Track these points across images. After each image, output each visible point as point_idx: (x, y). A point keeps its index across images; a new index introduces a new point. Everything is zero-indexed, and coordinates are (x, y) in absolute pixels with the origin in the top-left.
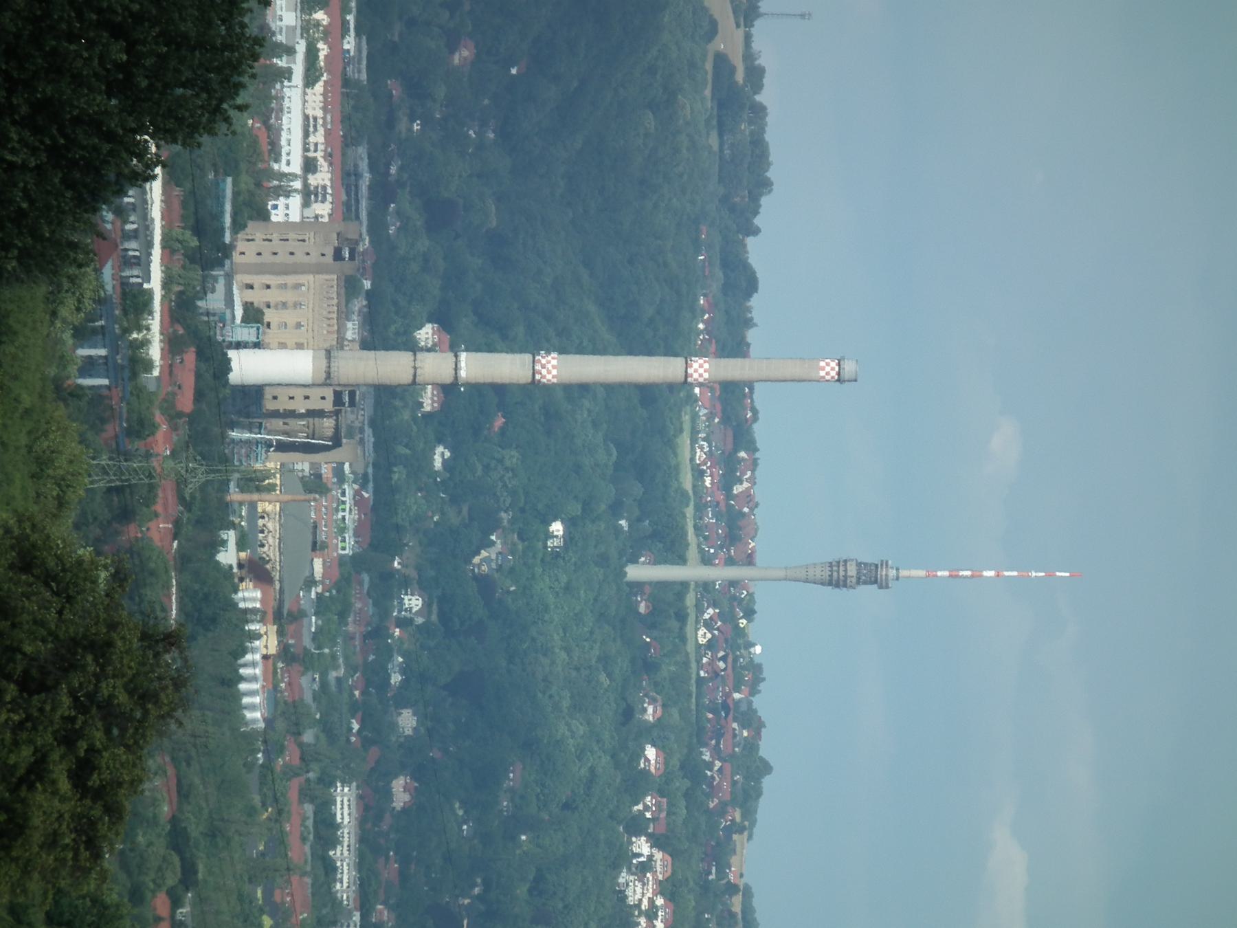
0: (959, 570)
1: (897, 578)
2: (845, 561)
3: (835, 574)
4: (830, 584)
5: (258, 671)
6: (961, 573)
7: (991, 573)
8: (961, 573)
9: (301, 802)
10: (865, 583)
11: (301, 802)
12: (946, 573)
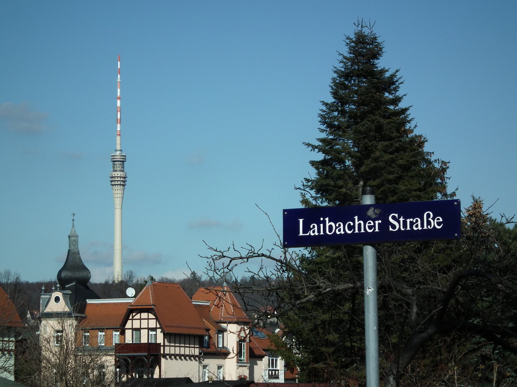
0: (117, 119)
1: (121, 151)
2: (124, 185)
3: (119, 183)
4: (430, 153)
5: (425, 228)
6: (119, 117)
7: (119, 102)
8: (119, 117)
9: (126, 296)
10: (123, 167)
11: (126, 296)
12: (119, 125)
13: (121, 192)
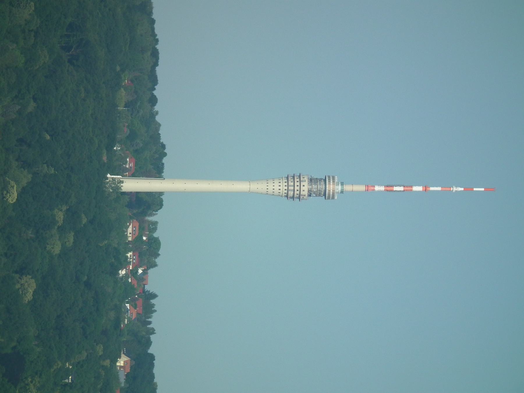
1: (342, 192)
13: (276, 191)
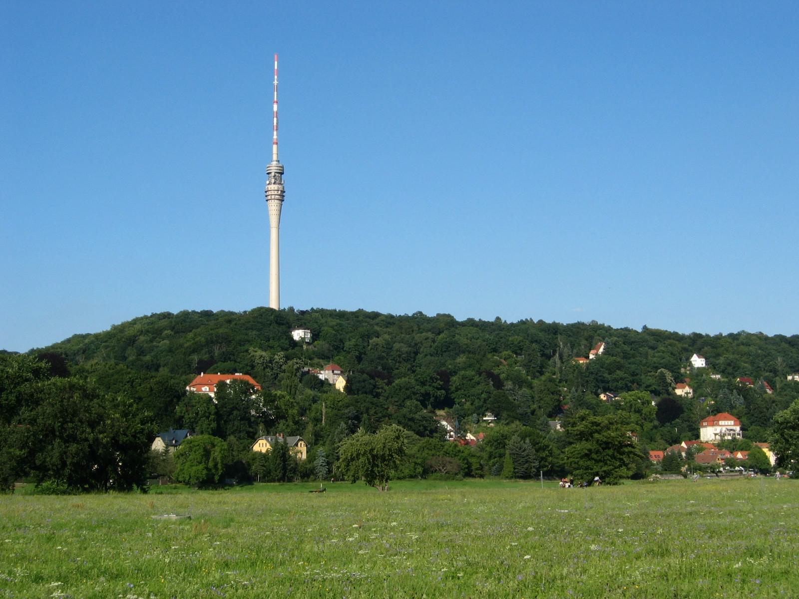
1: (278, 161)
